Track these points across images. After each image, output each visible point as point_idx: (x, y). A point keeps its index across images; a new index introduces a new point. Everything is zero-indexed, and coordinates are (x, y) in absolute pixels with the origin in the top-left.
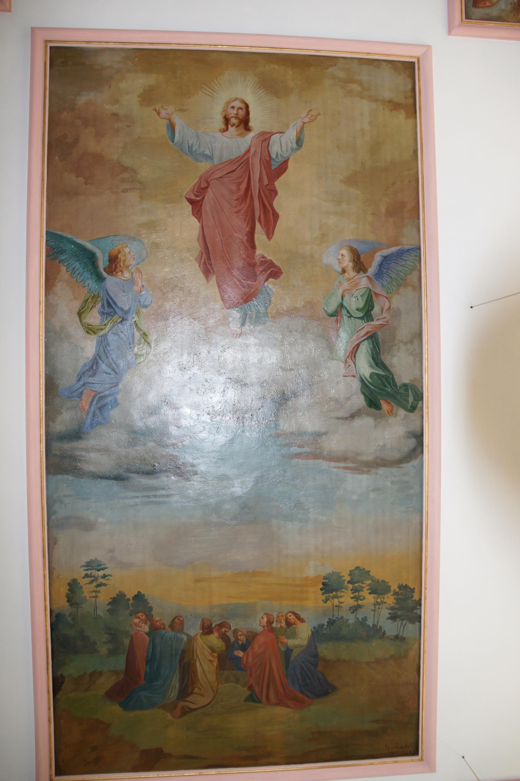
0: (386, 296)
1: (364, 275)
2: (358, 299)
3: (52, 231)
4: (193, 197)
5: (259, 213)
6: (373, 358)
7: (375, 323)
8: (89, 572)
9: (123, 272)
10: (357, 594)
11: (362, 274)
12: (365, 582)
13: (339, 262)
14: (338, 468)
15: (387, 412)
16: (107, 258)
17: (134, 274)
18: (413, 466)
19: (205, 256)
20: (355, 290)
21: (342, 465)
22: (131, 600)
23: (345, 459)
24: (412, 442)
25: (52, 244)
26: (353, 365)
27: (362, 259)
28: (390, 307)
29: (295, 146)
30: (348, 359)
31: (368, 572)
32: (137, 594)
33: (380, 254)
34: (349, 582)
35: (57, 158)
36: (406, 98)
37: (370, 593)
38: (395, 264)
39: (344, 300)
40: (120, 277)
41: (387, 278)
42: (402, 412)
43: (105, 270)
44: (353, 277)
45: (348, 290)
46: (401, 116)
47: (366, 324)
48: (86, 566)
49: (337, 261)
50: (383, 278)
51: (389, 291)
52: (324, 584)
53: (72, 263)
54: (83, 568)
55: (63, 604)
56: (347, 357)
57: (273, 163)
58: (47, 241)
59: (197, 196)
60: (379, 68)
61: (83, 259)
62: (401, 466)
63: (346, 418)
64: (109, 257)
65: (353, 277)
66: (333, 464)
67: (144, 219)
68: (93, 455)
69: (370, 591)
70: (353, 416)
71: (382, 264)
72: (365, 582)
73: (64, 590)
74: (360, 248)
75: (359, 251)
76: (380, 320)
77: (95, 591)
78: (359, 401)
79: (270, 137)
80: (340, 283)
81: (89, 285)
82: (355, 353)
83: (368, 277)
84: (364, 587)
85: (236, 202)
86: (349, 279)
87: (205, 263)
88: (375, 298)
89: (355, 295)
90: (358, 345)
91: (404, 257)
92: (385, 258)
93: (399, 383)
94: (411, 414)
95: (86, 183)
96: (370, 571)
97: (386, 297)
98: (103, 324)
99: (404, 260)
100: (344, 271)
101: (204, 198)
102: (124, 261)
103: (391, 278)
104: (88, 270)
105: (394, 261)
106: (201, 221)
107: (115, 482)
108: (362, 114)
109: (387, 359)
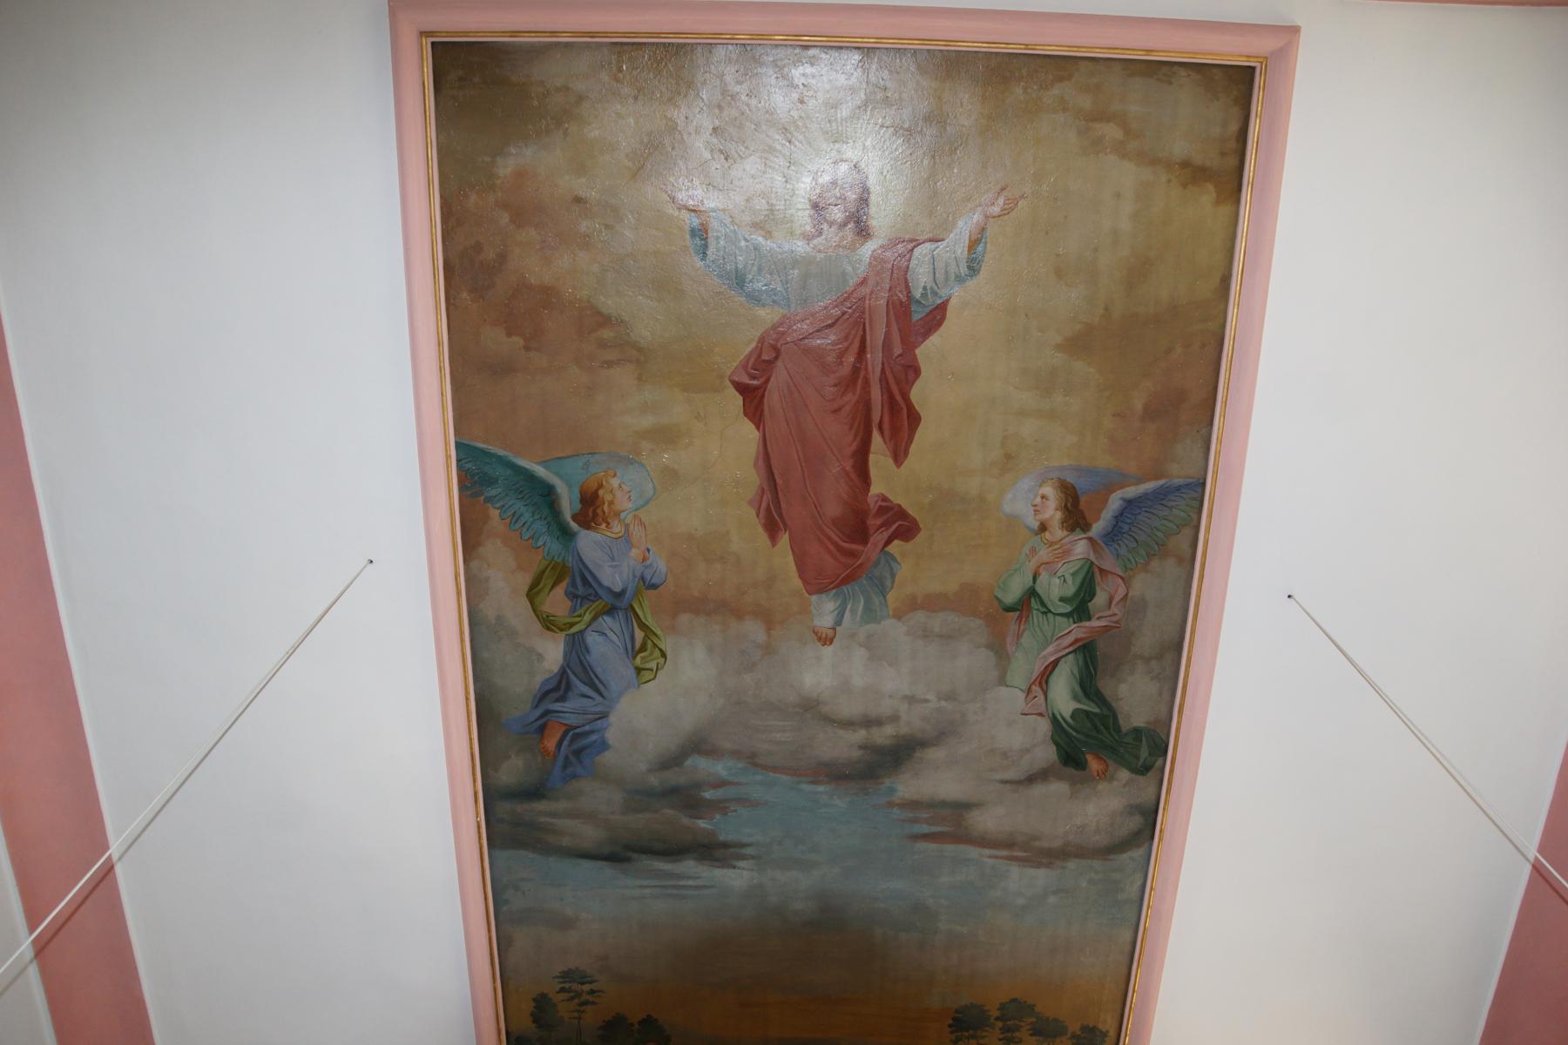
0: (1120, 574)
1: (1084, 536)
2: (1065, 581)
3: (466, 442)
4: (746, 380)
5: (879, 414)
6: (1082, 685)
7: (1095, 623)
8: (567, 986)
9: (608, 523)
10: (1009, 1035)
11: (1079, 535)
12: (1025, 1019)
13: (1035, 511)
14: (996, 857)
15: (1095, 774)
16: (576, 496)
17: (632, 526)
18: (1132, 859)
19: (768, 496)
20: (1060, 565)
21: (1005, 853)
22: (637, 1026)
23: (1010, 845)
24: (1135, 822)
25: (468, 466)
26: (1042, 697)
27: (1082, 506)
28: (1127, 595)
29: (964, 270)
30: (1033, 687)
31: (1032, 1007)
32: (645, 1017)
33: (1121, 496)
34: (997, 1019)
35: (465, 295)
36: (1223, 154)
37: (1031, 1035)
38: (1146, 514)
39: (1038, 582)
40: (605, 533)
41: (1127, 542)
42: (1124, 774)
43: (574, 518)
44: (1061, 540)
45: (1047, 563)
46: (1206, 197)
47: (1076, 625)
48: (562, 977)
49: (1033, 508)
50: (1120, 542)
51: (1129, 566)
52: (954, 1019)
53: (510, 504)
54: (557, 980)
55: (526, 1025)
56: (1033, 683)
57: (913, 308)
58: (458, 461)
59: (753, 377)
60: (1170, 83)
61: (530, 497)
62: (1112, 857)
63: (1019, 782)
64: (581, 493)
65: (1061, 540)
66: (987, 852)
67: (647, 422)
68: (561, 823)
69: (1031, 1032)
70: (1031, 779)
71: (1121, 514)
72: (1025, 1019)
73: (527, 1007)
74: (1080, 483)
75: (1078, 489)
76: (1103, 619)
77: (579, 1011)
78: (1047, 754)
79: (912, 250)
80: (1033, 551)
81: (544, 544)
82: (1048, 677)
83: (1090, 539)
84: (1021, 1027)
85: (836, 389)
86: (1051, 544)
87: (768, 509)
88: (1099, 578)
89: (1059, 574)
90: (1055, 663)
91: (1170, 500)
92: (1130, 504)
93: (1125, 726)
94: (1140, 778)
95: (527, 348)
96: (1034, 1005)
97: (1122, 578)
98: (576, 614)
99: (1166, 506)
100: (1043, 527)
101: (768, 380)
102: (611, 503)
103: (1137, 542)
104: (541, 518)
105: (1147, 509)
106: (761, 428)
107: (604, 863)
108: (1118, 195)
109: (1106, 686)
